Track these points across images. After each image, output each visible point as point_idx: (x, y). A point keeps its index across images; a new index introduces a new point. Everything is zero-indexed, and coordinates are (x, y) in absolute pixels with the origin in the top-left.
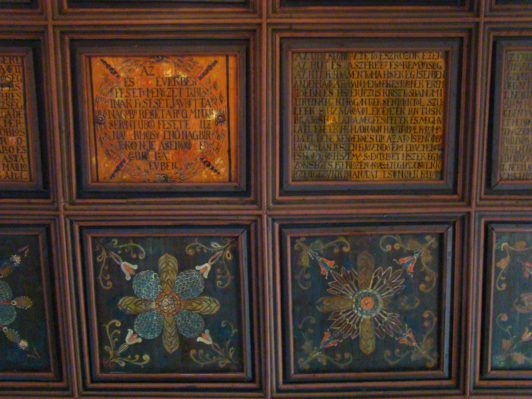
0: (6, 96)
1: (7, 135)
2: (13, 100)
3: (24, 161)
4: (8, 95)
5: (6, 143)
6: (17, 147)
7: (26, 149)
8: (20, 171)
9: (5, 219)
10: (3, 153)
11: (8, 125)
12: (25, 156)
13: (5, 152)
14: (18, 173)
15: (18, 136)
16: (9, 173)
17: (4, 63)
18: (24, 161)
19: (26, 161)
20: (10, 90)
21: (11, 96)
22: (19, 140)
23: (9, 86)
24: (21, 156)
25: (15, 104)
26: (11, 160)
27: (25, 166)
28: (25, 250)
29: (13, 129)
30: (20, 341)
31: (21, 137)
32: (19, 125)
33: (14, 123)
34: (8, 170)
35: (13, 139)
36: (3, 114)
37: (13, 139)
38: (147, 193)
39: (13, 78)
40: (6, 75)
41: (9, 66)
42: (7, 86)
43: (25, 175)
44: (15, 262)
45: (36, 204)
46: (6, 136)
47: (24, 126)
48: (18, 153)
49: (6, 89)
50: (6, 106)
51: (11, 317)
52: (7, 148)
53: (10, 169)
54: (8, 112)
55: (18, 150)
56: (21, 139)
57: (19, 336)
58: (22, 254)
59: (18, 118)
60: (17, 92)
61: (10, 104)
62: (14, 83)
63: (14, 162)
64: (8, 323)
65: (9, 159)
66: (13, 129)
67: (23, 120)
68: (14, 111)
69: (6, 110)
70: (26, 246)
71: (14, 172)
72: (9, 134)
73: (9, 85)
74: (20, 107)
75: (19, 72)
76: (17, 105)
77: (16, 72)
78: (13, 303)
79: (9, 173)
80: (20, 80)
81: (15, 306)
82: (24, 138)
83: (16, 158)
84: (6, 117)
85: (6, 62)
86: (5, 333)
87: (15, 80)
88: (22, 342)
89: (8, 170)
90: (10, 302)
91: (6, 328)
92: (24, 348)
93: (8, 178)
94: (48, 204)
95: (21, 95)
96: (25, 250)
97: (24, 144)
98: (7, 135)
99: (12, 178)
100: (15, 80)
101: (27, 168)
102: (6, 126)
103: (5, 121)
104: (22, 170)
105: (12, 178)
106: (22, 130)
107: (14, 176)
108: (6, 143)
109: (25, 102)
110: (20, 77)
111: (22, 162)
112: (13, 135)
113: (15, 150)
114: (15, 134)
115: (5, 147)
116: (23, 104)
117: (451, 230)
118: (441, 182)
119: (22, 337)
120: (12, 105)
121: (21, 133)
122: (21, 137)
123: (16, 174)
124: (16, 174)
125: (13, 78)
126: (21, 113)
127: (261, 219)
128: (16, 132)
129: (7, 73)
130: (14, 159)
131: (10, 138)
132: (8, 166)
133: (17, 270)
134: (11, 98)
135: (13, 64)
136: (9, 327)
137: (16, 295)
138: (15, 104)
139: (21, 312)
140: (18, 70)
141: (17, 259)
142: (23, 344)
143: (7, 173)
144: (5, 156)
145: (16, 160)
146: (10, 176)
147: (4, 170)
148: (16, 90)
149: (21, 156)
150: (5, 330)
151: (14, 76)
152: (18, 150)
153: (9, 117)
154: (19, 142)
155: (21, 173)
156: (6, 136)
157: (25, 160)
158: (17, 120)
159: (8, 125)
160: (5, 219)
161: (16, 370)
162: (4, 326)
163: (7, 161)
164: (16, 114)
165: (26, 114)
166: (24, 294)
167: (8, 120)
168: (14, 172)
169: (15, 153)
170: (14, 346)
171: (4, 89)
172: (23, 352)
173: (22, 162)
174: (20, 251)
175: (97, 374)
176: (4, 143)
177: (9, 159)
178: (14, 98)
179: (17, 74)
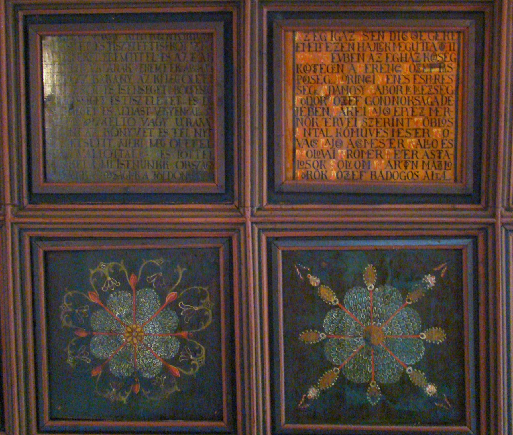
0: (436, 79)
1: (431, 126)
2: (443, 83)
3: (449, 158)
4: (437, 77)
5: (429, 136)
6: (442, 141)
7: (453, 143)
8: (443, 170)
9: (423, 229)
10: (424, 147)
11: (434, 114)
12: (451, 151)
13: (426, 146)
14: (440, 172)
15: (445, 127)
16: (429, 172)
17: (436, 39)
18: (449, 158)
19: (452, 157)
20: (440, 72)
21: (440, 80)
22: (446, 131)
23: (440, 68)
24: (446, 151)
25: (445, 88)
26: (433, 156)
27: (450, 164)
28: (442, 268)
29: (439, 119)
30: (427, 386)
31: (448, 128)
32: (447, 114)
33: (441, 112)
34: (428, 169)
35: (438, 131)
36: (429, 100)
37: (438, 131)
38: (404, 195)
39: (446, 57)
40: (437, 54)
41: (442, 43)
42: (435, 67)
43: (449, 174)
44: (429, 283)
45: (462, 209)
46: (429, 127)
47: (453, 115)
48: (443, 147)
49: (436, 70)
50: (433, 91)
51: (418, 353)
52: (430, 142)
53: (430, 166)
54: (436, 98)
55: (443, 144)
56: (448, 131)
57: (427, 379)
58: (437, 274)
59: (447, 106)
60: (448, 74)
61: (439, 89)
62: (446, 64)
63: (437, 159)
64: (412, 362)
65: (430, 155)
66: (439, 119)
67: (452, 108)
68: (442, 96)
69: (433, 96)
70: (443, 263)
71: (435, 172)
72: (434, 124)
73: (440, 66)
74: (450, 92)
75: (454, 50)
76: (447, 89)
77: (450, 50)
78: (422, 336)
79: (429, 172)
80: (453, 60)
81: (424, 341)
82: (452, 129)
83: (440, 153)
84: (432, 104)
85: (439, 38)
86: (408, 375)
87: (448, 59)
88: (430, 386)
89: (428, 169)
90: (418, 334)
91: (410, 368)
92: (431, 395)
93: (427, 179)
94: (478, 210)
95: (454, 79)
96: (442, 268)
97: (452, 137)
98: (431, 126)
99: (432, 179)
100: (448, 59)
101: (453, 166)
102: (430, 115)
103: (431, 109)
104: (445, 169)
105: (432, 179)
106: (450, 120)
107: (435, 176)
108: (429, 136)
109: (457, 87)
110: (454, 56)
111: (446, 159)
112: (439, 126)
113: (440, 143)
114: (441, 125)
115: (428, 141)
116: (454, 88)
117: (236, 235)
118: (294, 182)
119: (431, 380)
120: (441, 89)
121: (448, 123)
122: (448, 128)
123: (437, 174)
124: (437, 174)
125: (446, 57)
126: (451, 98)
127: (245, 228)
128: (442, 122)
129: (439, 51)
130: (437, 155)
131: (435, 130)
132: (428, 164)
133: (430, 294)
134: (441, 82)
135: (447, 41)
136: (413, 366)
137: (426, 325)
138: (445, 88)
139: (431, 347)
140: (452, 48)
141: (431, 280)
142: (431, 389)
143: (426, 173)
144: (426, 152)
145: (439, 157)
146: (430, 177)
147: (423, 169)
148: (448, 72)
149: (446, 151)
150: (410, 370)
151: (447, 55)
152: (443, 144)
153: (435, 104)
154: (446, 135)
155: (444, 173)
156: (429, 127)
157: (450, 156)
158: (445, 108)
159: (434, 114)
160: (423, 229)
161: (419, 423)
162: (408, 366)
163: (428, 158)
164: (444, 99)
165: (457, 101)
166: (436, 326)
167: (434, 108)
168: (435, 172)
169: (439, 147)
170: (418, 391)
171: (433, 70)
172: (431, 400)
173: (446, 159)
174: (435, 269)
175: (282, 425)
176: (426, 135)
177: (430, 155)
178: (445, 82)
179: (450, 53)
